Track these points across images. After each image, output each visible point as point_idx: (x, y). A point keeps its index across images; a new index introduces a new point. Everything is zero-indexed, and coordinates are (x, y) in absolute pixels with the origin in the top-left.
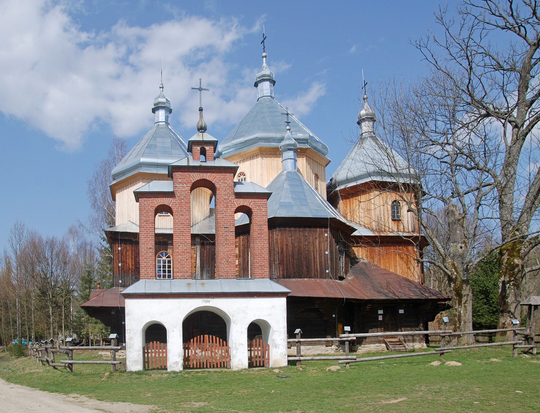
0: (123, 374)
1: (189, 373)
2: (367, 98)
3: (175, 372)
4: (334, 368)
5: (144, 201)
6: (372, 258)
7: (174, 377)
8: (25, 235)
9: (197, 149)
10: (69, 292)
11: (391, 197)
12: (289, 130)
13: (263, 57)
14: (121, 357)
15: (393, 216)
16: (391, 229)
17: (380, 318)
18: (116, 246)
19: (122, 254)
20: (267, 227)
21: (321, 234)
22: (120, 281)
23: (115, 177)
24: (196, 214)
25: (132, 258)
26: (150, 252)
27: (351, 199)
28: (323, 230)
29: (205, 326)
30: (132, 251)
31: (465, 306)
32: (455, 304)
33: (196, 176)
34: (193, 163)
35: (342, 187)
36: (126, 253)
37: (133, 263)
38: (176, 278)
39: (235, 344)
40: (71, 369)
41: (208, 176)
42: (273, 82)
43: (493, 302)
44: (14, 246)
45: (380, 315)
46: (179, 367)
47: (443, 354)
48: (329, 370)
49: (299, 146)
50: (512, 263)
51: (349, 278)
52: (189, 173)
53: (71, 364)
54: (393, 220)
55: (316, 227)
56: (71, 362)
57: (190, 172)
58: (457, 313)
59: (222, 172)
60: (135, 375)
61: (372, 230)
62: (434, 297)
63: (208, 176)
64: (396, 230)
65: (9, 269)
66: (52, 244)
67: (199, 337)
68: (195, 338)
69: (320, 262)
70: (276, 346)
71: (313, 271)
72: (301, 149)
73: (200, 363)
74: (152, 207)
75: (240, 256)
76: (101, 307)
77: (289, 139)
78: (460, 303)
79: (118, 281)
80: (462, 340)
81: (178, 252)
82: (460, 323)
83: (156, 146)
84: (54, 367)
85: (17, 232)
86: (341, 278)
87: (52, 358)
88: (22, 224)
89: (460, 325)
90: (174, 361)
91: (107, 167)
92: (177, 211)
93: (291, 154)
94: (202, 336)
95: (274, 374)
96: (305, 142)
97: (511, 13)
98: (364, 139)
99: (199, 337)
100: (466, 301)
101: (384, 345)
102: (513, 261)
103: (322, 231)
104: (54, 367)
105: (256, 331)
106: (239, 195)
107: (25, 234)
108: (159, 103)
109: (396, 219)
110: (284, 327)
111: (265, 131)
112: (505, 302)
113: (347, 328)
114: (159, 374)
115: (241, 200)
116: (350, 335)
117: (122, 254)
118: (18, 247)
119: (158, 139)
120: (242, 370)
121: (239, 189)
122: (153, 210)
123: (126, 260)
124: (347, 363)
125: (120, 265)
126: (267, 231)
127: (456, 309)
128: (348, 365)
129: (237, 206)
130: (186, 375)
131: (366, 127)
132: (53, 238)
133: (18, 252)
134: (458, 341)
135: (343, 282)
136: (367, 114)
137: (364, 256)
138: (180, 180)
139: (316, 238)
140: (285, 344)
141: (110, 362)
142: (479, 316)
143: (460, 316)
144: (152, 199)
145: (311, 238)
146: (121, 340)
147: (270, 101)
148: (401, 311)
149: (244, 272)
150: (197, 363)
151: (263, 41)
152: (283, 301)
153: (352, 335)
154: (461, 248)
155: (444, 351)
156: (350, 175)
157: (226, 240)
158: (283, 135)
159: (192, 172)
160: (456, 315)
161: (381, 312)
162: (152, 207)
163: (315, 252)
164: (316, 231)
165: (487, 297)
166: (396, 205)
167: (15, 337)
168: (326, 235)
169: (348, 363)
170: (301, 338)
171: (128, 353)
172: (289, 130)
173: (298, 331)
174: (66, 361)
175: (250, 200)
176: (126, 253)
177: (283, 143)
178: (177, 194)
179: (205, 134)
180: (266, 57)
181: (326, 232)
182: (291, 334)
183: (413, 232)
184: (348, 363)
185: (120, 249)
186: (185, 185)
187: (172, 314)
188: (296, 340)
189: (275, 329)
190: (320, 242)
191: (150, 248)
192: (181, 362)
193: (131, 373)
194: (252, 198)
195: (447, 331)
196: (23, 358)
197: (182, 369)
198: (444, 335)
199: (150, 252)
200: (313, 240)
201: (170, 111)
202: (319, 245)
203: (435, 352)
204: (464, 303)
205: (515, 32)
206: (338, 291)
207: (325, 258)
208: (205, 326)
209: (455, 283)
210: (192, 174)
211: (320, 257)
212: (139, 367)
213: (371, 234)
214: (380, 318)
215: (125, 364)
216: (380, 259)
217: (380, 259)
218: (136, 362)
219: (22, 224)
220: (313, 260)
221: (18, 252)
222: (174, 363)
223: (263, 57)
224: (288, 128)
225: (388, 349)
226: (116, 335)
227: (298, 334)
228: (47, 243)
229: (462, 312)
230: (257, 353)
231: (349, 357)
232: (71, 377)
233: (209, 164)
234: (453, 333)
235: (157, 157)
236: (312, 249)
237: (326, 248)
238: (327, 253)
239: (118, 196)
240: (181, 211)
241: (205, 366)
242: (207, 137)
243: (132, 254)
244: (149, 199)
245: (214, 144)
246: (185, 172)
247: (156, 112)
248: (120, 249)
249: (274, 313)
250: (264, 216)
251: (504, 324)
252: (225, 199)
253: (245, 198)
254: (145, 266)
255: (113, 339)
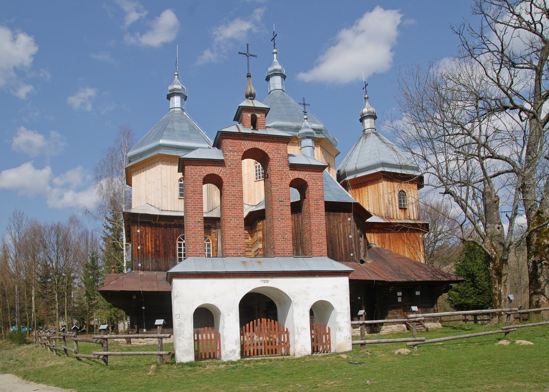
0: (171, 366)
1: (249, 362)
2: (368, 98)
3: (232, 362)
4: (405, 351)
5: (191, 169)
6: (383, 243)
7: (233, 368)
8: (24, 223)
9: (247, 116)
10: (71, 279)
11: (397, 186)
12: (307, 119)
13: (274, 53)
14: (142, 344)
15: (400, 205)
16: (399, 217)
17: (400, 300)
18: (134, 229)
19: (141, 237)
20: (290, 211)
21: (345, 219)
22: (140, 265)
23: (130, 159)
24: (215, 199)
25: (151, 241)
26: (199, 226)
27: (360, 189)
28: (347, 214)
29: (259, 309)
30: (152, 234)
31: (505, 285)
32: (495, 283)
33: (248, 145)
34: (243, 130)
35: (352, 177)
36: (145, 236)
37: (153, 247)
38: (229, 256)
39: (298, 328)
40: (106, 362)
41: (260, 145)
42: (284, 77)
43: (479, 285)
44: (13, 234)
45: (400, 296)
46: (236, 357)
47: (508, 332)
48: (399, 353)
49: (316, 135)
50: (543, 244)
51: (369, 262)
52: (240, 141)
53: (106, 356)
54: (400, 208)
55: (340, 211)
56: (106, 353)
57: (240, 139)
58: (497, 292)
59: (275, 142)
60: (186, 366)
61: (382, 217)
62: (446, 279)
63: (260, 145)
64: (403, 218)
65: (6, 257)
66: (58, 230)
67: (255, 321)
68: (251, 322)
69: (345, 246)
70: (340, 329)
71: (338, 254)
72: (318, 138)
73: (257, 350)
74: (200, 176)
75: (263, 240)
76: (121, 291)
77: (307, 127)
78: (500, 282)
79: (138, 265)
80: (503, 319)
81: (230, 227)
82: (500, 301)
83: (174, 130)
84: (78, 359)
85: (16, 220)
86: (362, 262)
87: (76, 348)
88: (21, 212)
89: (501, 303)
90: (230, 349)
91: (113, 155)
92: (228, 182)
93: (309, 142)
94: (259, 320)
95: (343, 360)
96: (319, 132)
97: (530, 11)
98: (367, 134)
99: (255, 321)
100: (506, 280)
101: (404, 326)
102: (543, 241)
103: (345, 215)
104: (78, 359)
105: (319, 312)
106: (294, 167)
107: (24, 222)
108: (175, 89)
109: (403, 208)
110: (347, 309)
111: (282, 120)
112: (537, 281)
113: (415, 308)
114: (215, 364)
115: (296, 172)
116: (418, 315)
117: (141, 237)
118: (17, 235)
119: (175, 123)
120: (305, 357)
121: (293, 161)
122: (201, 179)
123: (146, 243)
124: (414, 346)
125: (139, 248)
126: (290, 216)
127: (496, 288)
128: (416, 347)
129: (292, 179)
130: (246, 365)
131: (368, 123)
132: (58, 224)
133: (17, 240)
134: (499, 320)
135: (364, 265)
136: (369, 112)
137: (376, 242)
138: (230, 148)
139: (340, 222)
140: (349, 326)
141: (156, 353)
142: (466, 297)
143: (500, 295)
144: (200, 167)
145: (336, 222)
146: (169, 325)
147: (281, 94)
148: (418, 293)
149: (300, 248)
150: (254, 350)
151: (274, 39)
152: (344, 281)
153: (420, 315)
154: (499, 228)
155: (510, 330)
156: (359, 166)
157: (282, 214)
158: (299, 124)
159: (243, 140)
160: (496, 294)
161: (399, 294)
162: (200, 176)
163: (340, 236)
164: (340, 215)
165: (473, 281)
166: (402, 195)
167: (14, 324)
168: (349, 219)
169: (416, 345)
170: (366, 320)
171: (174, 340)
172: (307, 119)
173: (361, 312)
174: (100, 353)
175: (306, 173)
176: (145, 236)
177: (301, 132)
178: (228, 163)
179: (254, 101)
180: (276, 53)
181: (349, 216)
182: (354, 315)
183: (419, 219)
184: (416, 345)
185: (139, 231)
186: (236, 154)
187: (227, 296)
188: (361, 322)
189: (338, 311)
190: (344, 226)
191: (199, 222)
192: (239, 350)
193: (182, 364)
194: (307, 171)
195: (513, 309)
196: (26, 346)
197: (239, 358)
198: (510, 313)
199: (199, 226)
200: (337, 224)
201: (186, 98)
202: (343, 229)
203: (501, 331)
204: (504, 282)
205: (530, 30)
206: (365, 274)
207: (349, 241)
208: (259, 309)
209: (494, 262)
210: (243, 142)
211: (345, 241)
212: (190, 358)
213: (382, 221)
214: (400, 300)
215: (173, 356)
216: (390, 245)
217: (390, 245)
218: (186, 352)
219: (21, 212)
220: (338, 244)
221: (17, 240)
222: (230, 352)
223: (274, 53)
224: (305, 117)
225: (408, 329)
226: (163, 320)
227: (362, 316)
228: (52, 228)
229: (502, 291)
230: (206, 335)
231: (418, 339)
232: (108, 372)
233: (260, 132)
234: (519, 311)
235: (177, 140)
236: (337, 233)
237: (349, 232)
238: (350, 237)
239: (134, 179)
240: (232, 182)
241: (252, 354)
242: (257, 104)
243: (151, 237)
244: (197, 167)
245: (265, 111)
246: (235, 139)
247: (171, 99)
248: (139, 231)
249: (336, 292)
250: (320, 190)
251: (538, 302)
252: (279, 171)
253: (300, 171)
254: (193, 242)
255: (160, 325)
